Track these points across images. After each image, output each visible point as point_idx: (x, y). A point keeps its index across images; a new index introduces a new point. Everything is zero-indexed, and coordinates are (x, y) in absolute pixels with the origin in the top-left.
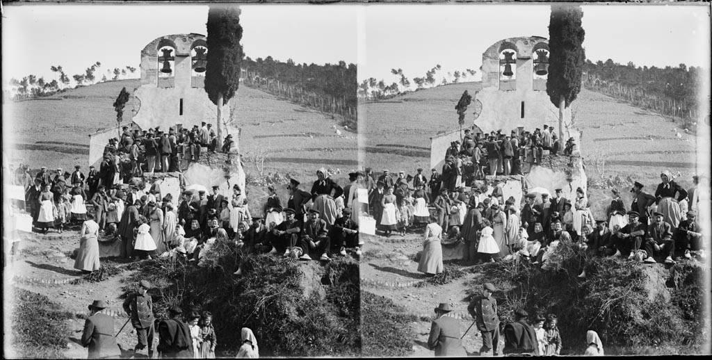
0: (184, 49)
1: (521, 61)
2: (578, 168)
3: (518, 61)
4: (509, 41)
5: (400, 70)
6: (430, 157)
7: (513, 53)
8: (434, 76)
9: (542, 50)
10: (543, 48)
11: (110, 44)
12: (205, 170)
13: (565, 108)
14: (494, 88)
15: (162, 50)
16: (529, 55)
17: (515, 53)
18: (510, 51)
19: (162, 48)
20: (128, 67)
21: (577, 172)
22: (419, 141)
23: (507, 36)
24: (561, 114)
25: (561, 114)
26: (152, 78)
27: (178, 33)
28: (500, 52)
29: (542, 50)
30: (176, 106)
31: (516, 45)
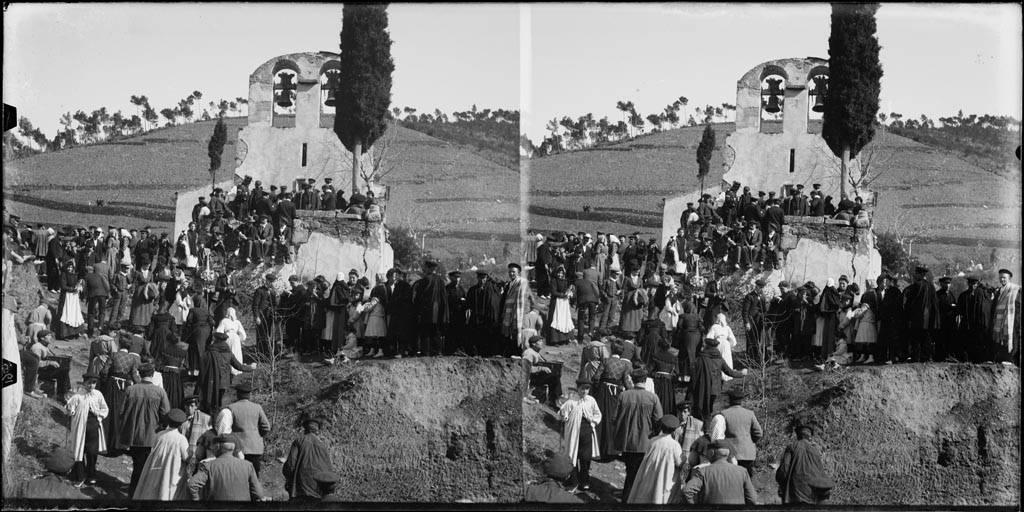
0: (798, 79)
1: (304, 87)
2: (865, 244)
3: (787, 92)
4: (775, 64)
5: (630, 104)
6: (661, 227)
7: (293, 75)
8: (192, 108)
9: (334, 71)
10: (336, 68)
11: (205, 63)
12: (332, 243)
13: (851, 158)
14: (754, 129)
15: (767, 81)
16: (315, 78)
17: (784, 80)
18: (777, 77)
19: (768, 78)
20: (724, 105)
21: (375, 244)
22: (647, 204)
23: (772, 57)
24: (843, 166)
25: (843, 166)
26: (263, 113)
27: (789, 58)
28: (274, 73)
29: (334, 71)
30: (297, 154)
31: (785, 69)
